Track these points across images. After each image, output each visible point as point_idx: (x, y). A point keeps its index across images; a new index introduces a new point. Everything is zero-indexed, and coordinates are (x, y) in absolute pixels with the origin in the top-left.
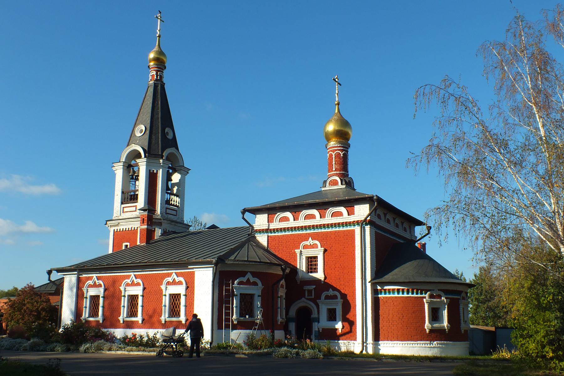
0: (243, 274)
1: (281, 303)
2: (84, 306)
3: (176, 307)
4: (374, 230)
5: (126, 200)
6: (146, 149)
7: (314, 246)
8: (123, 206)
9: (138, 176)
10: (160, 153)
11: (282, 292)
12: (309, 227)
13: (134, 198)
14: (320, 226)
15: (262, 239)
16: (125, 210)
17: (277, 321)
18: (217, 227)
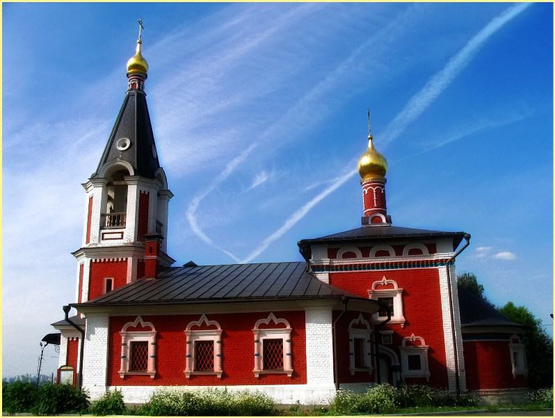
2: (256, 352)
7: (391, 286)
8: (103, 231)
12: (382, 266)
16: (106, 236)
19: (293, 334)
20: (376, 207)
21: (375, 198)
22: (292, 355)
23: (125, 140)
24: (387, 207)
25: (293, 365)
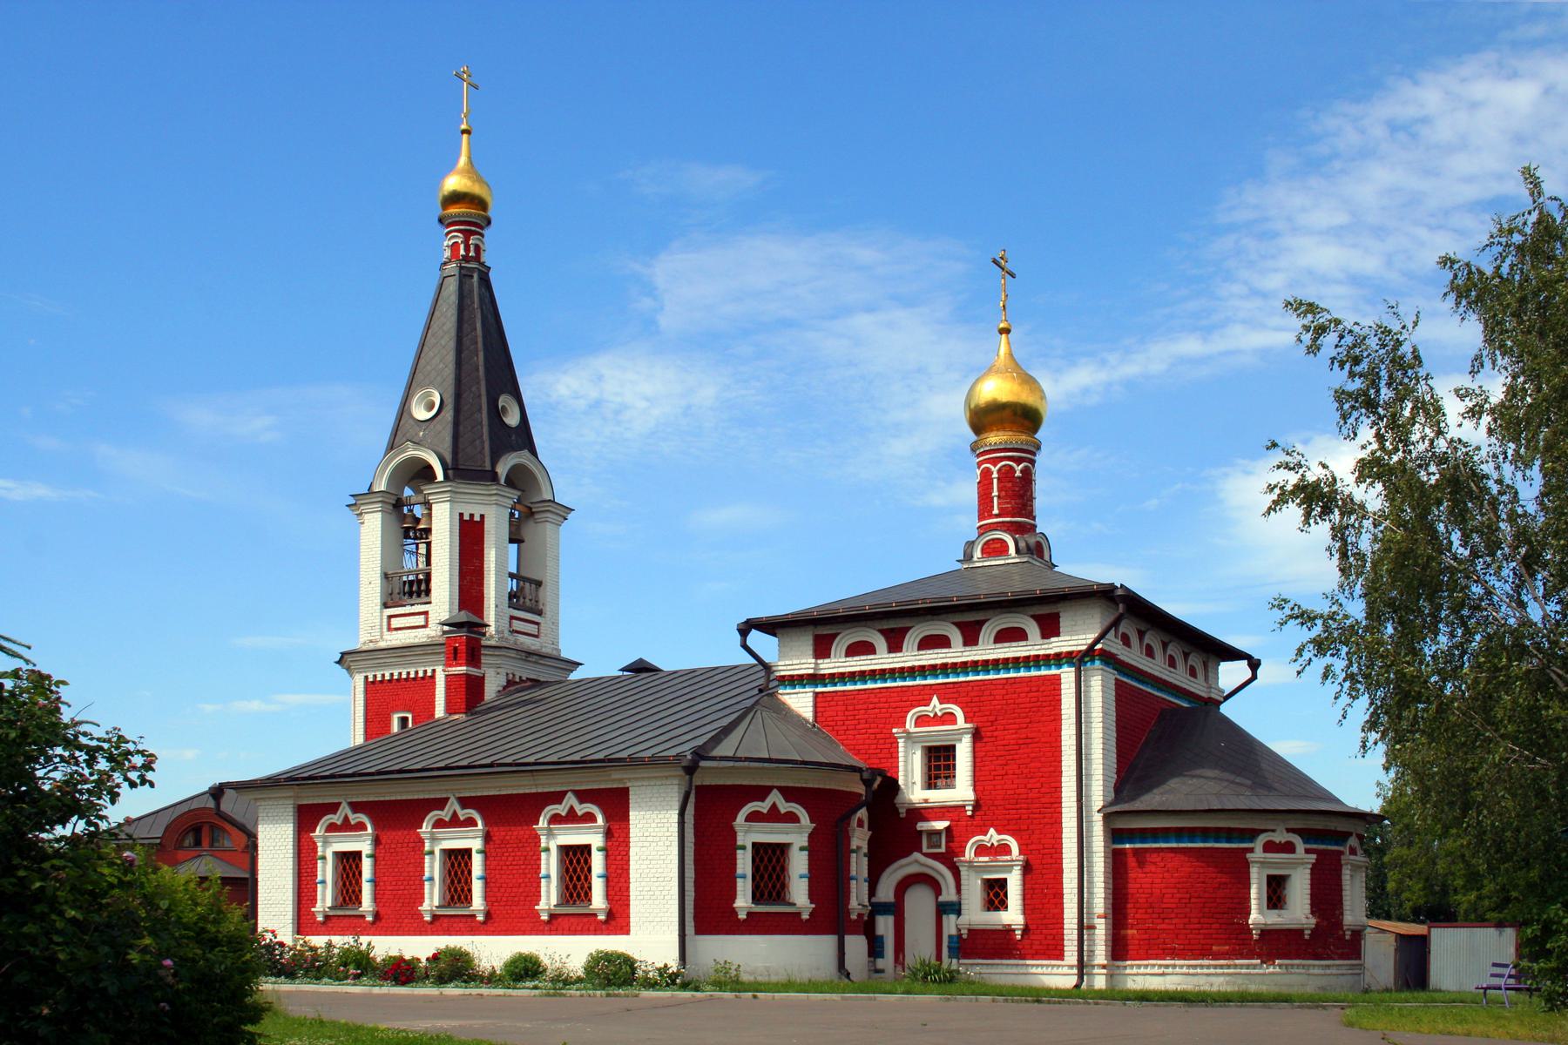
0: (761, 793)
1: (859, 866)
3: (579, 879)
4: (1113, 675)
5: (396, 596)
6: (448, 458)
7: (949, 718)
9: (428, 531)
10: (488, 468)
11: (860, 839)
12: (933, 670)
13: (419, 588)
14: (964, 667)
15: (801, 702)
16: (395, 623)
17: (848, 912)
18: (655, 670)
19: (609, 834)
20: (997, 516)
21: (995, 493)
22: (607, 878)
23: (430, 394)
24: (1037, 512)
25: (608, 896)
